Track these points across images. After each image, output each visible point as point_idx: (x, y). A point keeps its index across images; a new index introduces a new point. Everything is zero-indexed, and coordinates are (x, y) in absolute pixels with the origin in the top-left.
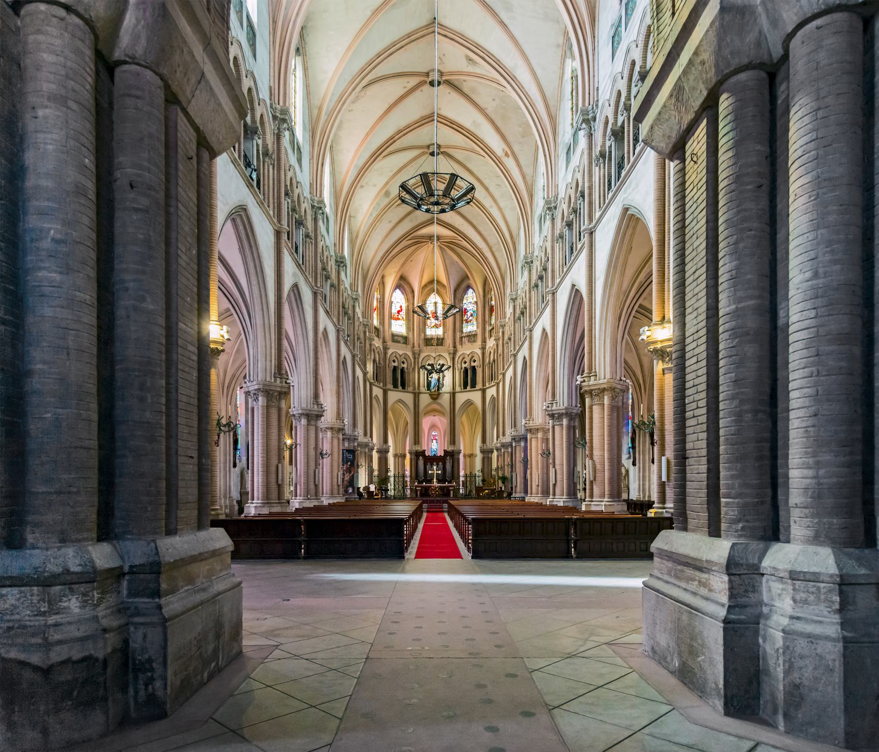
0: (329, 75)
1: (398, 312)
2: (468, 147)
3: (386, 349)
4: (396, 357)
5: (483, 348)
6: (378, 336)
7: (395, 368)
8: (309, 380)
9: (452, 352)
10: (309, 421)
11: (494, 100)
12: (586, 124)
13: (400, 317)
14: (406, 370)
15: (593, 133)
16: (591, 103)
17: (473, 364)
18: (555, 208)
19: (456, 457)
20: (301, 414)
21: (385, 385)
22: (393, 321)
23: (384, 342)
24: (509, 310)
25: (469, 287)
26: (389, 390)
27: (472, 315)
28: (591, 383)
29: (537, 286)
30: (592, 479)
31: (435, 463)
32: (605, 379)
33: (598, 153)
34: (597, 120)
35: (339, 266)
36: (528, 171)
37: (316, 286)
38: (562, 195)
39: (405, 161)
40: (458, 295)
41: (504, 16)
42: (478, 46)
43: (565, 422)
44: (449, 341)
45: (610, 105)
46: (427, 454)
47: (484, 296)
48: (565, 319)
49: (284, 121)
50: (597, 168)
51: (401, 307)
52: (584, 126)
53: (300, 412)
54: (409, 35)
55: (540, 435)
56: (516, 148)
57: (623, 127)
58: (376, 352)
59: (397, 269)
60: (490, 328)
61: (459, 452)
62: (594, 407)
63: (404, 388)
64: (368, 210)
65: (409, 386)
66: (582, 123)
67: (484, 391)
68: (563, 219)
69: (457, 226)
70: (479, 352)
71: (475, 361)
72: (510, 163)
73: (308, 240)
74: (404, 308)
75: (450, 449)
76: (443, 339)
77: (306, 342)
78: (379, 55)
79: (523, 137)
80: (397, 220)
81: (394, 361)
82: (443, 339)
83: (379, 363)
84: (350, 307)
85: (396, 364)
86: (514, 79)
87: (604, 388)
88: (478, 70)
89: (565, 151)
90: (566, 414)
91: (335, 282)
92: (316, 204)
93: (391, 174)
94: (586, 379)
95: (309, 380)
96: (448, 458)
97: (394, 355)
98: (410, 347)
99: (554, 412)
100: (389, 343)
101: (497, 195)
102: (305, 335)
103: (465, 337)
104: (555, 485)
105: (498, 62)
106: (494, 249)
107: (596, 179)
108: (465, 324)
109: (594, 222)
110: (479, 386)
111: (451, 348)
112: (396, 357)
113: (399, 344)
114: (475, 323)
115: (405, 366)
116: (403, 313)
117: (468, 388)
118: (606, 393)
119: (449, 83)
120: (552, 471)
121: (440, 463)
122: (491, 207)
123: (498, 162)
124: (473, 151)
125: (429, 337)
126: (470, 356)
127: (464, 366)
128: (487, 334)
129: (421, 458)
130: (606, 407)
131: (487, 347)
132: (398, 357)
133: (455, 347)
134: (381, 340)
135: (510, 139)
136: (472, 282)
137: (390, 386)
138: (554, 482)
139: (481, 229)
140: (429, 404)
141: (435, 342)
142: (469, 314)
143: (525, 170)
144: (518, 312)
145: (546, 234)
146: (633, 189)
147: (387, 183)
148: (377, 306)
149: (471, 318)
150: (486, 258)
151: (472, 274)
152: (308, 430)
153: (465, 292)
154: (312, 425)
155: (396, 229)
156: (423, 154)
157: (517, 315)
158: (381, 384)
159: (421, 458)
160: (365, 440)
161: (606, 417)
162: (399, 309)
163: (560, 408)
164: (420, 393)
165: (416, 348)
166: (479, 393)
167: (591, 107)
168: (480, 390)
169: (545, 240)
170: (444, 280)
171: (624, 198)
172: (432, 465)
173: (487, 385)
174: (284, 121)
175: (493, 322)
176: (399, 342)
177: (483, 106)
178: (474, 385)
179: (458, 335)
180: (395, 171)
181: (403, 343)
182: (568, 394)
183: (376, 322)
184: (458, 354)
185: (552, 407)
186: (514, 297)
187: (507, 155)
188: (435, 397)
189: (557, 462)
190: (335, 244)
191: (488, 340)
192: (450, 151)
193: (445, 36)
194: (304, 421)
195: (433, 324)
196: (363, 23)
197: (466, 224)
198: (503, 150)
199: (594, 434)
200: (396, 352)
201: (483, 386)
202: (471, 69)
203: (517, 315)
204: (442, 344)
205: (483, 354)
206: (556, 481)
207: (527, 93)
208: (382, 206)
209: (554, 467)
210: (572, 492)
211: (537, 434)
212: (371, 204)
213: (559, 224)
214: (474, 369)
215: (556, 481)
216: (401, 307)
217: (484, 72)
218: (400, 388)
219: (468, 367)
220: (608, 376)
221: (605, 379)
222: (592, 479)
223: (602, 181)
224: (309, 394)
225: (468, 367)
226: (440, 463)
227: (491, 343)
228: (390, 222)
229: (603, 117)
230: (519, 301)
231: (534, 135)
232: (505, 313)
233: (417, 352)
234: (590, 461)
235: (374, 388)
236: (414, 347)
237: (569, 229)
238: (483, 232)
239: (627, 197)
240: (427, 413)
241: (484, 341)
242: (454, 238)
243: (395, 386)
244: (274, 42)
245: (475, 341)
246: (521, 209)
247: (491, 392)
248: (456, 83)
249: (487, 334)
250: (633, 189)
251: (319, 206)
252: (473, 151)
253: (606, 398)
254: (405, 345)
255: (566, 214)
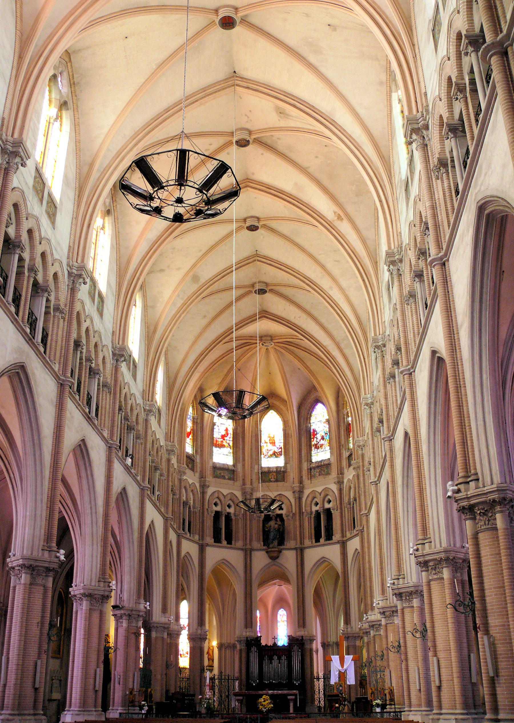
0: (106, 130)
1: (223, 437)
2: (293, 216)
3: (204, 486)
4: (218, 498)
5: (340, 483)
6: (193, 469)
7: (217, 515)
8: (38, 513)
9: (297, 489)
10: (33, 578)
11: (317, 157)
12: (417, 134)
13: (224, 443)
14: (233, 517)
15: (428, 143)
16: (420, 110)
17: (327, 506)
18: (401, 261)
19: (307, 647)
20: (23, 566)
21: (202, 537)
22: (215, 449)
23: (202, 477)
24: (367, 424)
25: (317, 401)
26: (207, 545)
27: (323, 438)
28: (471, 493)
29: (393, 376)
30: (491, 674)
31: (275, 657)
32: (492, 483)
33: (436, 161)
34: (430, 127)
35: (117, 361)
36: (369, 234)
37: (65, 376)
38: (406, 239)
39: (217, 239)
40: (304, 412)
41: (312, 58)
42: (287, 94)
43: (446, 573)
44: (292, 475)
45: (441, 100)
46: (263, 643)
47: (338, 411)
48: (429, 408)
49: (16, 154)
50: (439, 181)
51: (227, 430)
52: (414, 137)
53: (21, 562)
54: (204, 90)
55: (416, 602)
56: (350, 209)
57: (461, 119)
58: (189, 490)
59: (219, 380)
60: (348, 454)
61: (312, 640)
62: (481, 535)
63: (229, 542)
64: (170, 298)
65: (237, 540)
66: (411, 134)
67: (343, 544)
68: (411, 270)
69: (292, 319)
70: (334, 488)
71: (329, 502)
72: (345, 227)
73: (57, 314)
74: (231, 432)
75: (301, 633)
76: (284, 472)
77: (38, 453)
78: (167, 110)
79: (357, 196)
80: (213, 314)
81: (216, 504)
82: (284, 472)
83: (194, 508)
84: (141, 421)
85: (218, 508)
86: (333, 123)
87: (494, 501)
88: (292, 124)
89: (404, 188)
90: (447, 559)
91: (109, 380)
92: (75, 271)
93: (200, 254)
94: (462, 487)
95: (38, 513)
96: (296, 648)
97: (216, 495)
98: (239, 483)
99: (427, 558)
100: (210, 479)
101: (336, 271)
102: (36, 442)
103: (314, 468)
104: (439, 688)
105: (312, 108)
106: (342, 346)
107: (439, 195)
108: (314, 451)
109: (444, 247)
110: (337, 536)
111: (297, 484)
112: (218, 498)
113: (222, 481)
114: (328, 448)
115: (232, 510)
116: (229, 439)
117: (322, 540)
118: (498, 508)
119: (259, 142)
120: (433, 661)
121: (284, 658)
122: (331, 288)
123: (330, 227)
124: (299, 221)
125: (266, 470)
126: (322, 495)
127: (314, 508)
128: (344, 463)
129: (254, 649)
130: (501, 533)
131: (345, 481)
132: (222, 497)
133: (301, 482)
134: (197, 475)
135: (342, 199)
136: (320, 394)
137: (209, 539)
138: (437, 683)
139: (323, 321)
140: (267, 566)
141: (272, 477)
142: (319, 436)
143: (365, 233)
144: (376, 420)
145: (395, 302)
146: (485, 175)
147: (194, 266)
148: (193, 430)
149: (322, 442)
150: (333, 358)
151: (319, 384)
152: (30, 593)
153: (312, 408)
154: (37, 585)
155: (212, 326)
156: (238, 229)
157: (375, 426)
158: (197, 537)
159: (254, 649)
160: (163, 620)
161: (503, 552)
162: (224, 433)
163: (436, 550)
164: (252, 550)
165: (248, 486)
166: (337, 548)
167: (420, 113)
168: (338, 542)
169: (395, 309)
170: (282, 391)
171: (476, 194)
172: (271, 659)
173: (348, 535)
174: (16, 154)
175: (351, 446)
176: (223, 477)
177: (305, 164)
178: (329, 536)
179: (305, 466)
180: (204, 250)
181: (229, 479)
182: (447, 527)
183: (189, 449)
184: (307, 492)
185: (423, 549)
186: (370, 401)
187: (339, 218)
188: (275, 555)
189: (440, 645)
190: (113, 332)
191: (345, 471)
192: (273, 224)
193: (248, 88)
194: (25, 578)
195: (271, 453)
196: (147, 77)
197: (304, 316)
198: (335, 213)
199: (487, 585)
200: (218, 492)
201: (343, 536)
202: (283, 123)
203: (375, 426)
204: (283, 480)
205: (340, 490)
206: (440, 681)
207: (350, 136)
208: (189, 293)
209: (435, 655)
210: (471, 701)
211: (410, 601)
212: (174, 291)
213: (407, 278)
214: (328, 512)
215: (440, 681)
216: (227, 430)
217: (299, 125)
218: (225, 543)
219: (321, 510)
220: (497, 479)
221: (492, 484)
222: (491, 674)
223: (447, 194)
224: (37, 533)
225: (321, 510)
226: (284, 658)
227: (349, 475)
228: (205, 316)
229: (437, 117)
230: (376, 408)
231: (370, 192)
232: (363, 429)
233: (248, 490)
234: (485, 638)
235: (184, 543)
236: (244, 484)
237: (420, 281)
238: (326, 324)
239: (479, 191)
240: (263, 583)
241: (341, 473)
242: (293, 337)
243: (217, 539)
244: (17, 76)
245: (328, 474)
246: (364, 280)
247: (354, 545)
248: (269, 142)
249: (344, 463)
250: (485, 175)
251: (79, 273)
252: (299, 221)
253: (498, 516)
254: (231, 482)
255: (413, 263)
